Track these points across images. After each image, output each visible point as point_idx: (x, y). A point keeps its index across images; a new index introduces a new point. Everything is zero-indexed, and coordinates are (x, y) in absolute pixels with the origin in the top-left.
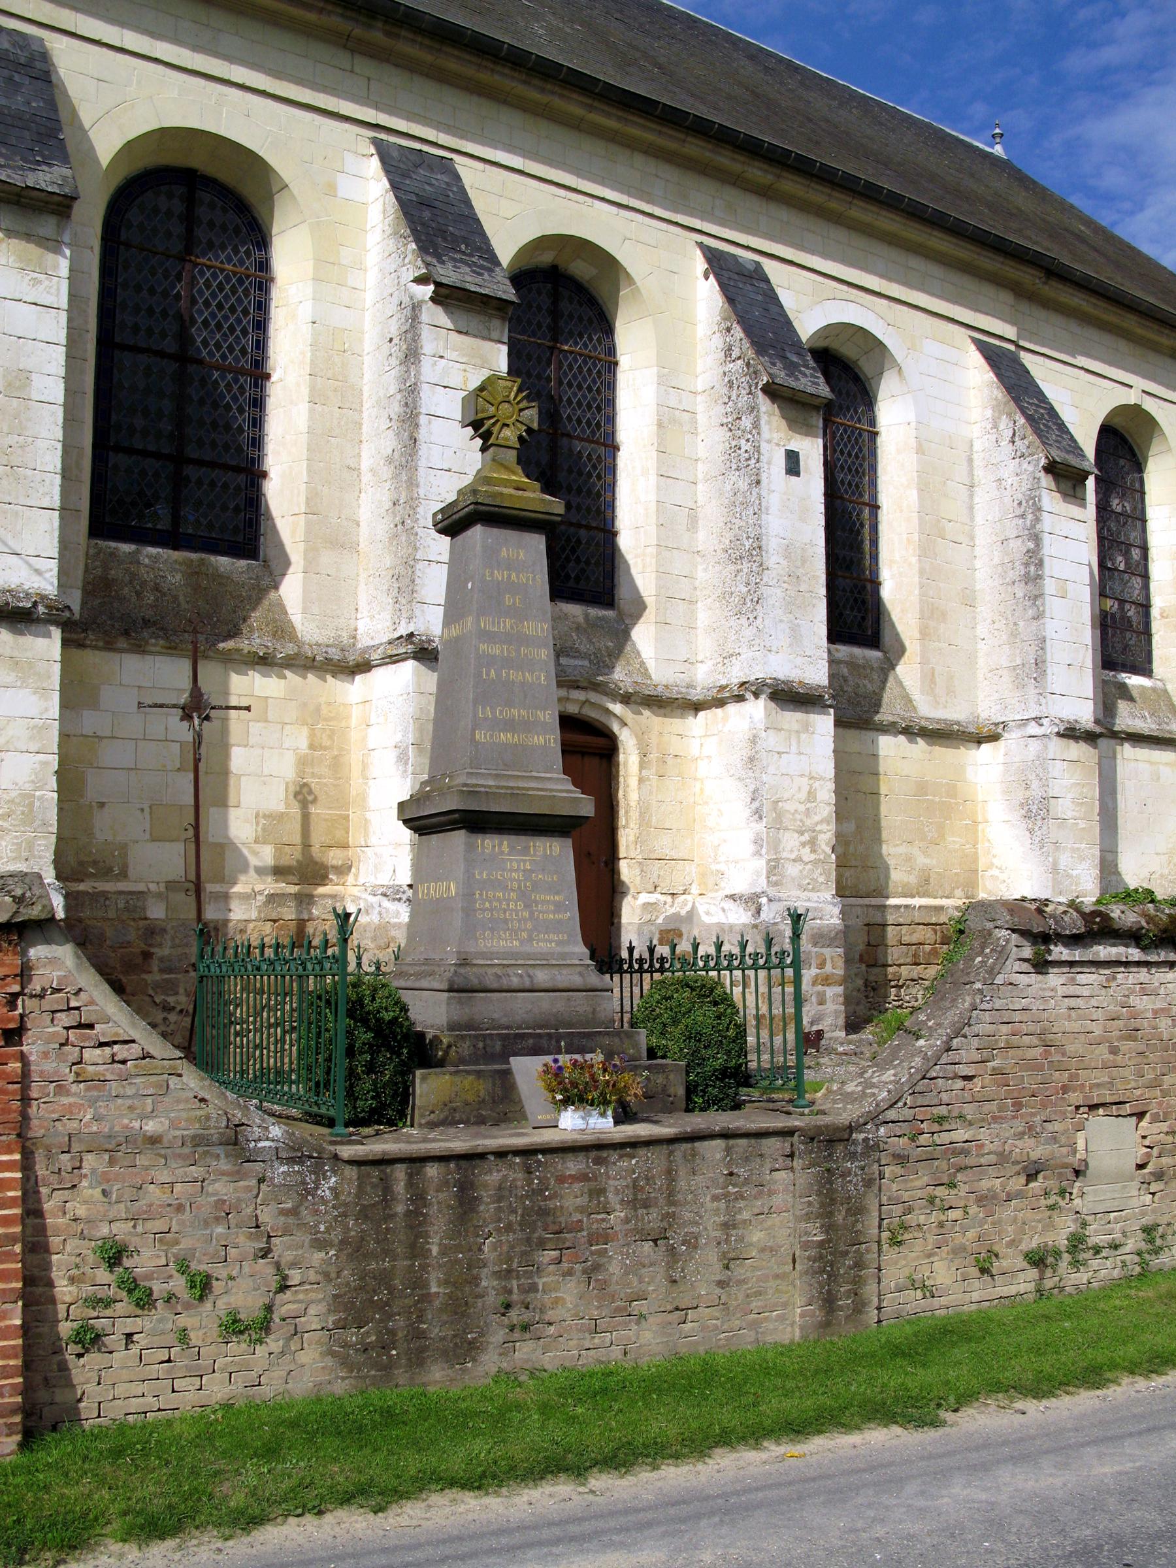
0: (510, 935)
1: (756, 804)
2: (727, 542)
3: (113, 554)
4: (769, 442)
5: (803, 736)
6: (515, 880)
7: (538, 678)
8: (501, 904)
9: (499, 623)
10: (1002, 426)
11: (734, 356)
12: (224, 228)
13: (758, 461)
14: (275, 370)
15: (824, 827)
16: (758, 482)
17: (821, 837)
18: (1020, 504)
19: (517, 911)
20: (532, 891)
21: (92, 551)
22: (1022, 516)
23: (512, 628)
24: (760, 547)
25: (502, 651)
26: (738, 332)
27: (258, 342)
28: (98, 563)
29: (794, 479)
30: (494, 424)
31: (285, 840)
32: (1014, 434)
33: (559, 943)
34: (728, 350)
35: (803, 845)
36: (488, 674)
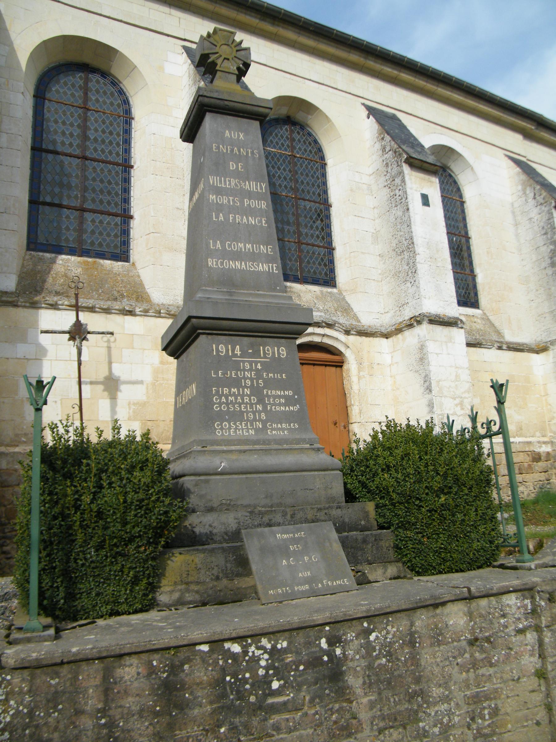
0: (246, 425)
1: (427, 383)
2: (395, 245)
3: (41, 259)
4: (411, 189)
5: (449, 345)
6: (248, 378)
7: (260, 221)
8: (236, 399)
9: (225, 181)
10: (528, 192)
11: (387, 150)
12: (105, 93)
13: (407, 198)
14: (135, 163)
15: (466, 395)
16: (408, 209)
17: (466, 401)
18: (543, 228)
19: (251, 405)
20: (264, 387)
21: (27, 257)
22: (546, 234)
23: (236, 185)
24: (413, 243)
25: (229, 201)
26: (388, 138)
27: (126, 150)
28: (31, 263)
29: (426, 208)
30: (218, 58)
31: (148, 418)
32: (535, 195)
33: (290, 430)
34: (384, 149)
35: (456, 405)
36: (217, 217)
